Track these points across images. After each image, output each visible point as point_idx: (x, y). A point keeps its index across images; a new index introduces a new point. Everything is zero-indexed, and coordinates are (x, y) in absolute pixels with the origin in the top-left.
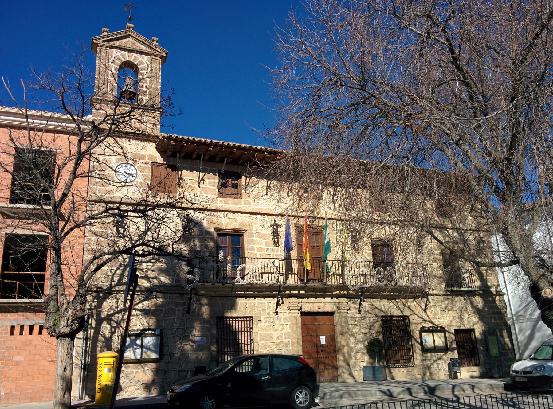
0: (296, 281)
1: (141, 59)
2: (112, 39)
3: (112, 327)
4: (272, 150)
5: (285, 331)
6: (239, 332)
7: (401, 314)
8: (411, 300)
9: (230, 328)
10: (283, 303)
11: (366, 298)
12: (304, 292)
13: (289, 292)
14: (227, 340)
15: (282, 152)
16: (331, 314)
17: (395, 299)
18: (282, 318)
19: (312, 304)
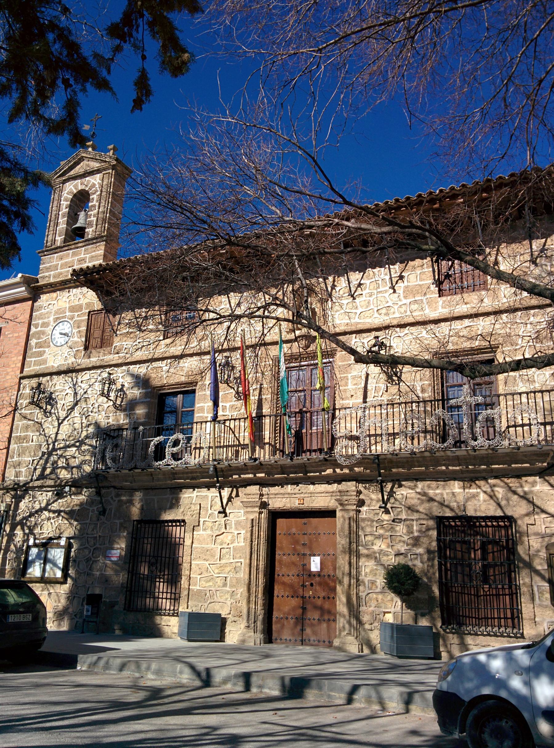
0: (267, 457)
1: (93, 181)
2: (65, 171)
3: (25, 534)
4: (114, 263)
5: (236, 544)
6: (180, 544)
7: (499, 513)
8: (530, 479)
9: (167, 538)
10: (237, 495)
11: (406, 480)
12: (263, 475)
13: (237, 476)
14: (162, 557)
15: (129, 260)
16: (330, 514)
17: (485, 479)
18: (233, 522)
19: (283, 498)
